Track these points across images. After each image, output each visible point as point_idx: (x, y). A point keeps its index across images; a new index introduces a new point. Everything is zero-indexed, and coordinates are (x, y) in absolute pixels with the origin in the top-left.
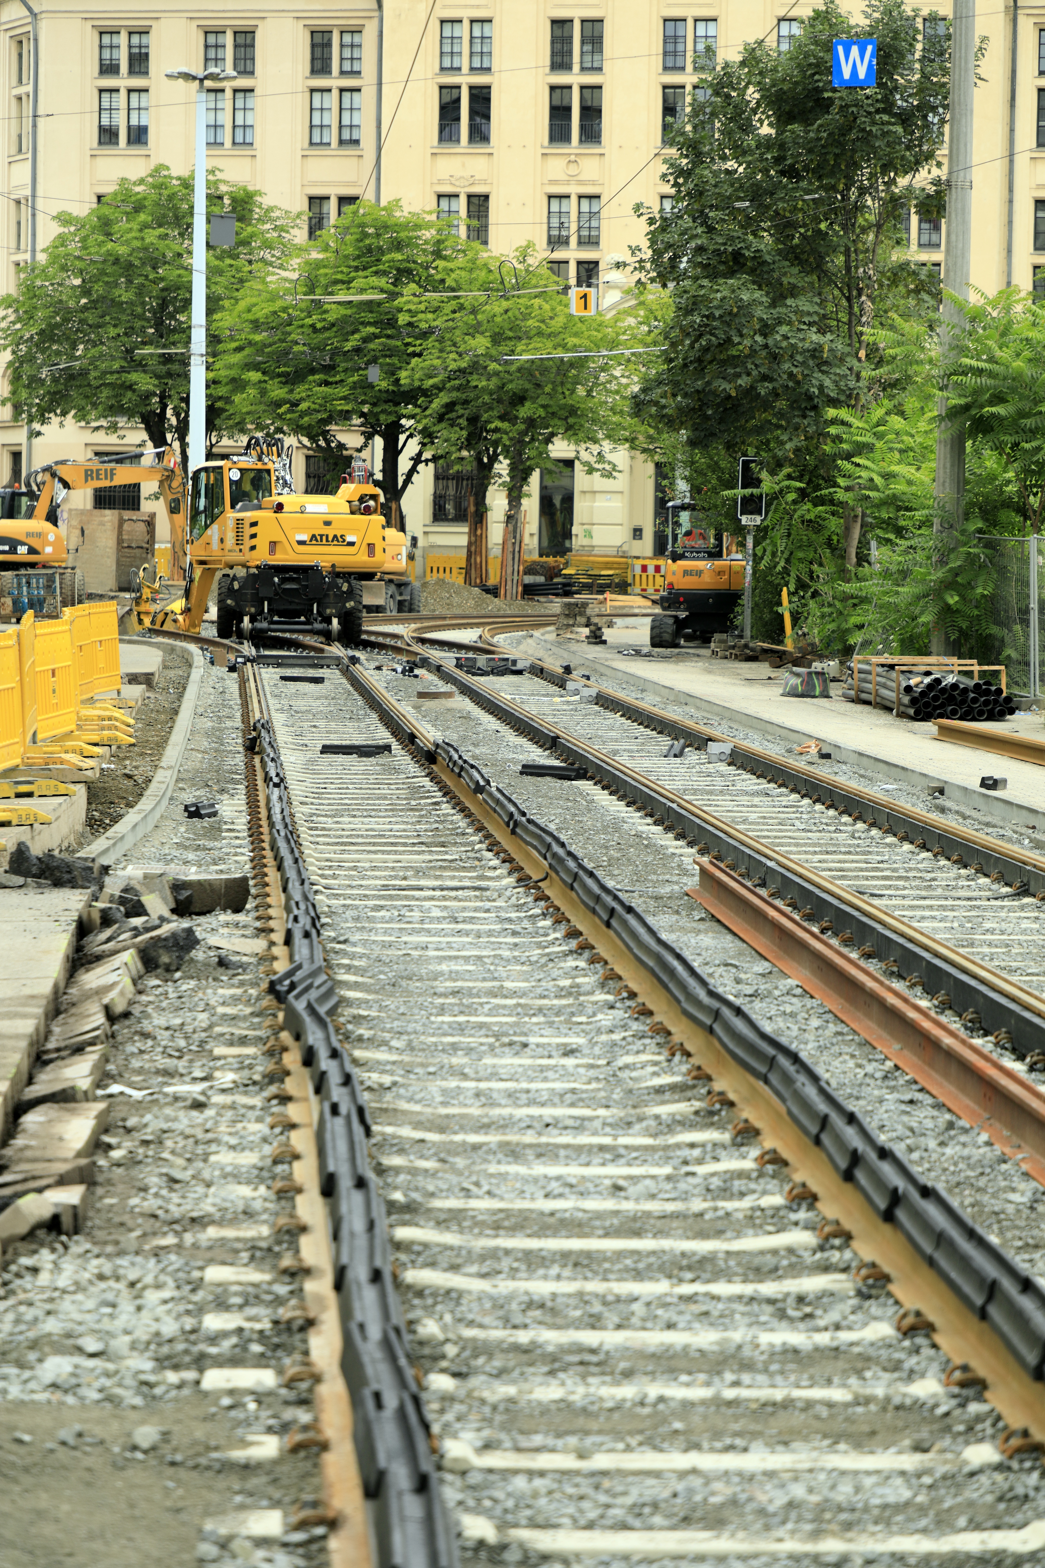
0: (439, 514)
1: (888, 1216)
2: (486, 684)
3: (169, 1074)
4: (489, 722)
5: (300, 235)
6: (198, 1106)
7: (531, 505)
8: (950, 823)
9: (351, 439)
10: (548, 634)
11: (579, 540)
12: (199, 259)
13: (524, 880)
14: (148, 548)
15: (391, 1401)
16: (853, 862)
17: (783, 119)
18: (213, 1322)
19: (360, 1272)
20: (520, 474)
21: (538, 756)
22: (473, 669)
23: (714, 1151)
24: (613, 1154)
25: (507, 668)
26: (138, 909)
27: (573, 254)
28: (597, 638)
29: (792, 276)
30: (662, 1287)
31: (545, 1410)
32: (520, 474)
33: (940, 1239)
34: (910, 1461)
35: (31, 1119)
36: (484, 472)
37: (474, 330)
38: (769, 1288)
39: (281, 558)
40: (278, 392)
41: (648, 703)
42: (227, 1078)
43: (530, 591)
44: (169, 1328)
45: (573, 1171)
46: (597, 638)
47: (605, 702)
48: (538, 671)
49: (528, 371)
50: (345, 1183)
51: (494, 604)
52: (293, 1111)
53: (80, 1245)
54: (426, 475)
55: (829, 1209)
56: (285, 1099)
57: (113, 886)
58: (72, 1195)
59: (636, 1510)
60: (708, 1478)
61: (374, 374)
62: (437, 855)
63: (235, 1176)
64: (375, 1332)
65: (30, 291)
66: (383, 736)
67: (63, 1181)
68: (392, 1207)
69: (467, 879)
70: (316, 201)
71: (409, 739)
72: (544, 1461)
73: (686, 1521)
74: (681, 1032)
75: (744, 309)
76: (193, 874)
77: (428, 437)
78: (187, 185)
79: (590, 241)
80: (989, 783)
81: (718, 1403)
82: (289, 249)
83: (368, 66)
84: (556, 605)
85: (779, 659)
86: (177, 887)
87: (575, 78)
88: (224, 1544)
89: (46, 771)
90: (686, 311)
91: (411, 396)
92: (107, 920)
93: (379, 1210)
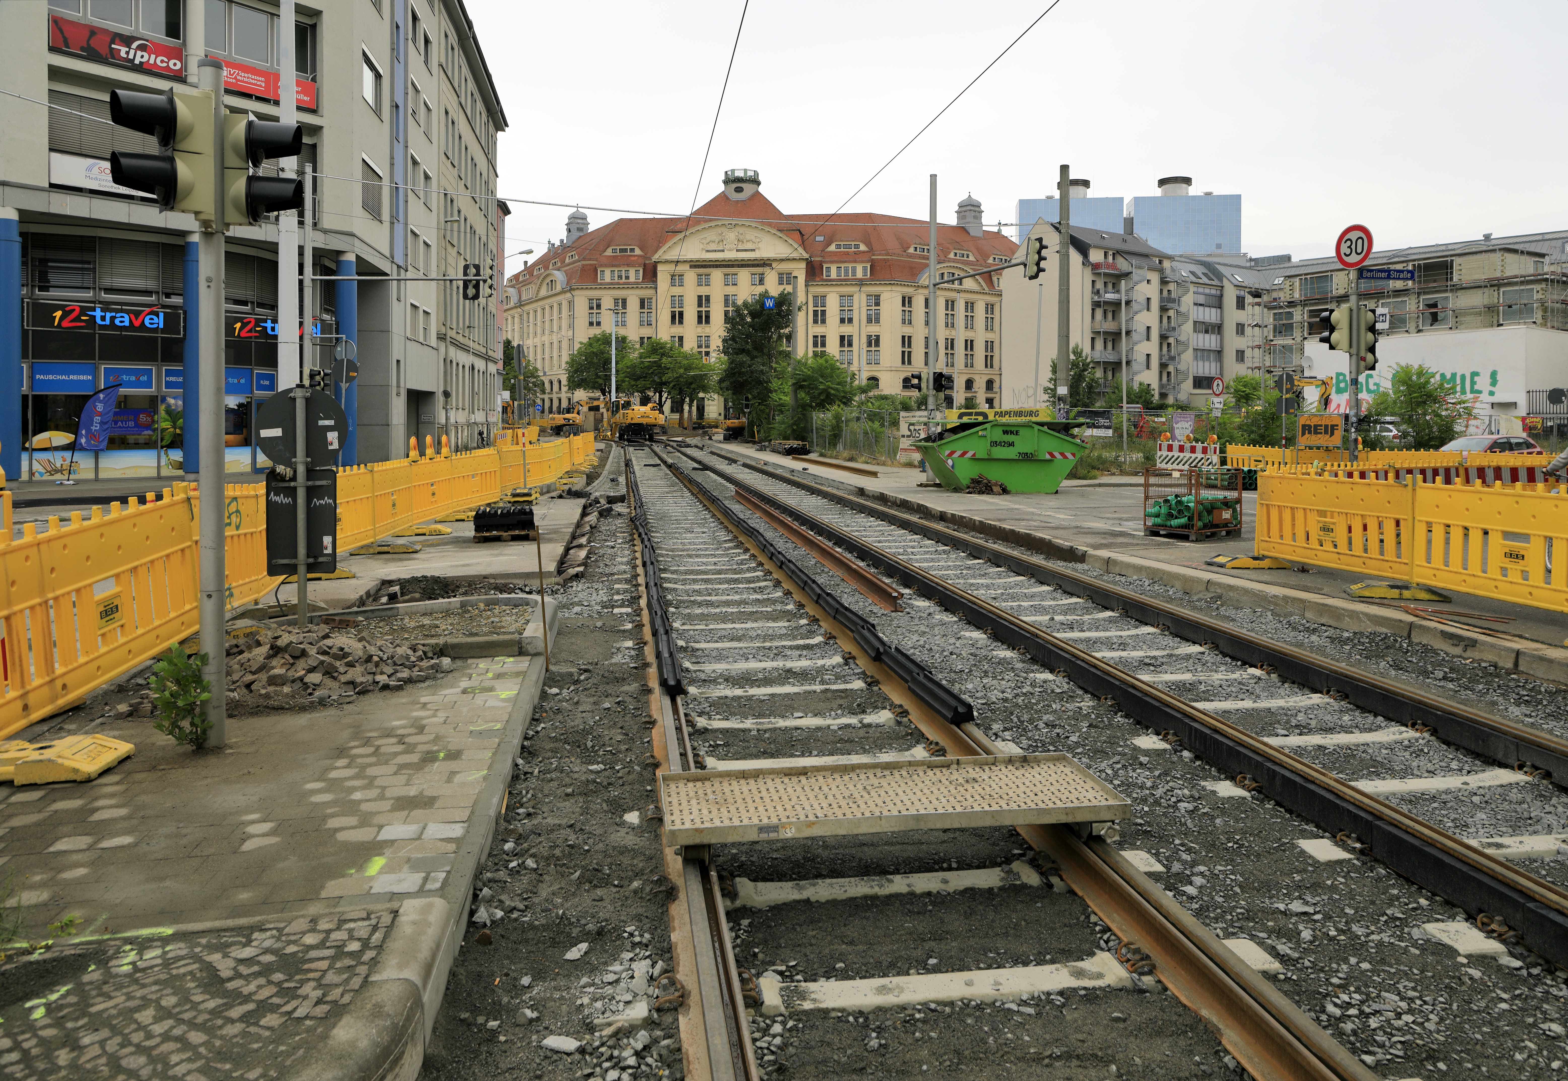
0: (672, 411)
1: (781, 567)
2: (683, 449)
3: (606, 540)
4: (685, 458)
5: (638, 346)
6: (613, 547)
7: (694, 408)
8: (795, 478)
9: (651, 394)
10: (699, 438)
11: (706, 416)
12: (614, 352)
13: (693, 494)
14: (602, 420)
15: (659, 613)
16: (772, 488)
17: (753, 318)
18: (616, 597)
19: (652, 584)
20: (691, 401)
21: (696, 465)
22: (680, 446)
23: (739, 554)
24: (715, 556)
25: (689, 446)
26: (599, 502)
27: (703, 350)
28: (710, 439)
29: (755, 353)
30: (726, 586)
31: (697, 615)
32: (691, 401)
33: (793, 572)
34: (787, 624)
35: (571, 552)
36: (682, 402)
37: (680, 367)
38: (752, 585)
39: (633, 422)
40: (633, 383)
41: (723, 453)
42: (620, 541)
43: (694, 428)
44: (605, 599)
45: (705, 560)
46: (710, 439)
47: (712, 453)
48: (696, 446)
49: (694, 377)
50: (648, 563)
51: (686, 432)
52: (636, 548)
53: (583, 580)
54: (669, 402)
55: (766, 567)
56: (634, 545)
57: (592, 497)
58: (581, 569)
59: (720, 638)
60: (737, 630)
61: (656, 378)
62: (673, 489)
63: (622, 564)
64: (655, 597)
65: (572, 360)
66: (659, 462)
67: (579, 565)
68: (660, 570)
69: (679, 494)
70: (642, 339)
71: (665, 462)
72: (697, 627)
73: (732, 640)
74: (730, 527)
75: (744, 362)
76: (612, 494)
77: (669, 393)
78: (610, 335)
79: (708, 346)
80: (804, 469)
81: (740, 612)
82: (635, 350)
83: (654, 307)
84: (701, 431)
85: (754, 443)
86: (608, 497)
87: (703, 309)
88: (618, 649)
89: (576, 472)
90: (731, 363)
91: (665, 383)
92: (591, 505)
93: (657, 570)
